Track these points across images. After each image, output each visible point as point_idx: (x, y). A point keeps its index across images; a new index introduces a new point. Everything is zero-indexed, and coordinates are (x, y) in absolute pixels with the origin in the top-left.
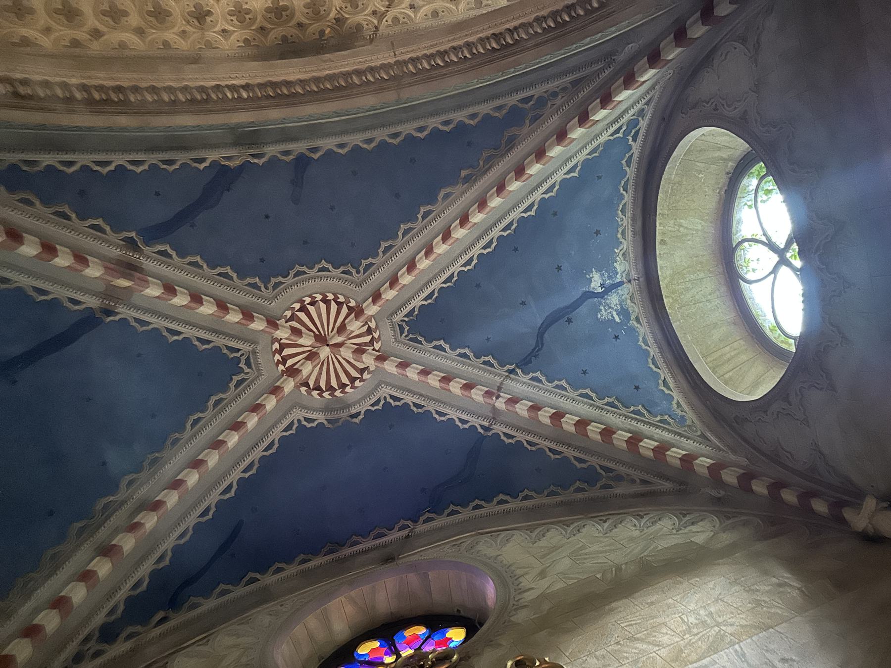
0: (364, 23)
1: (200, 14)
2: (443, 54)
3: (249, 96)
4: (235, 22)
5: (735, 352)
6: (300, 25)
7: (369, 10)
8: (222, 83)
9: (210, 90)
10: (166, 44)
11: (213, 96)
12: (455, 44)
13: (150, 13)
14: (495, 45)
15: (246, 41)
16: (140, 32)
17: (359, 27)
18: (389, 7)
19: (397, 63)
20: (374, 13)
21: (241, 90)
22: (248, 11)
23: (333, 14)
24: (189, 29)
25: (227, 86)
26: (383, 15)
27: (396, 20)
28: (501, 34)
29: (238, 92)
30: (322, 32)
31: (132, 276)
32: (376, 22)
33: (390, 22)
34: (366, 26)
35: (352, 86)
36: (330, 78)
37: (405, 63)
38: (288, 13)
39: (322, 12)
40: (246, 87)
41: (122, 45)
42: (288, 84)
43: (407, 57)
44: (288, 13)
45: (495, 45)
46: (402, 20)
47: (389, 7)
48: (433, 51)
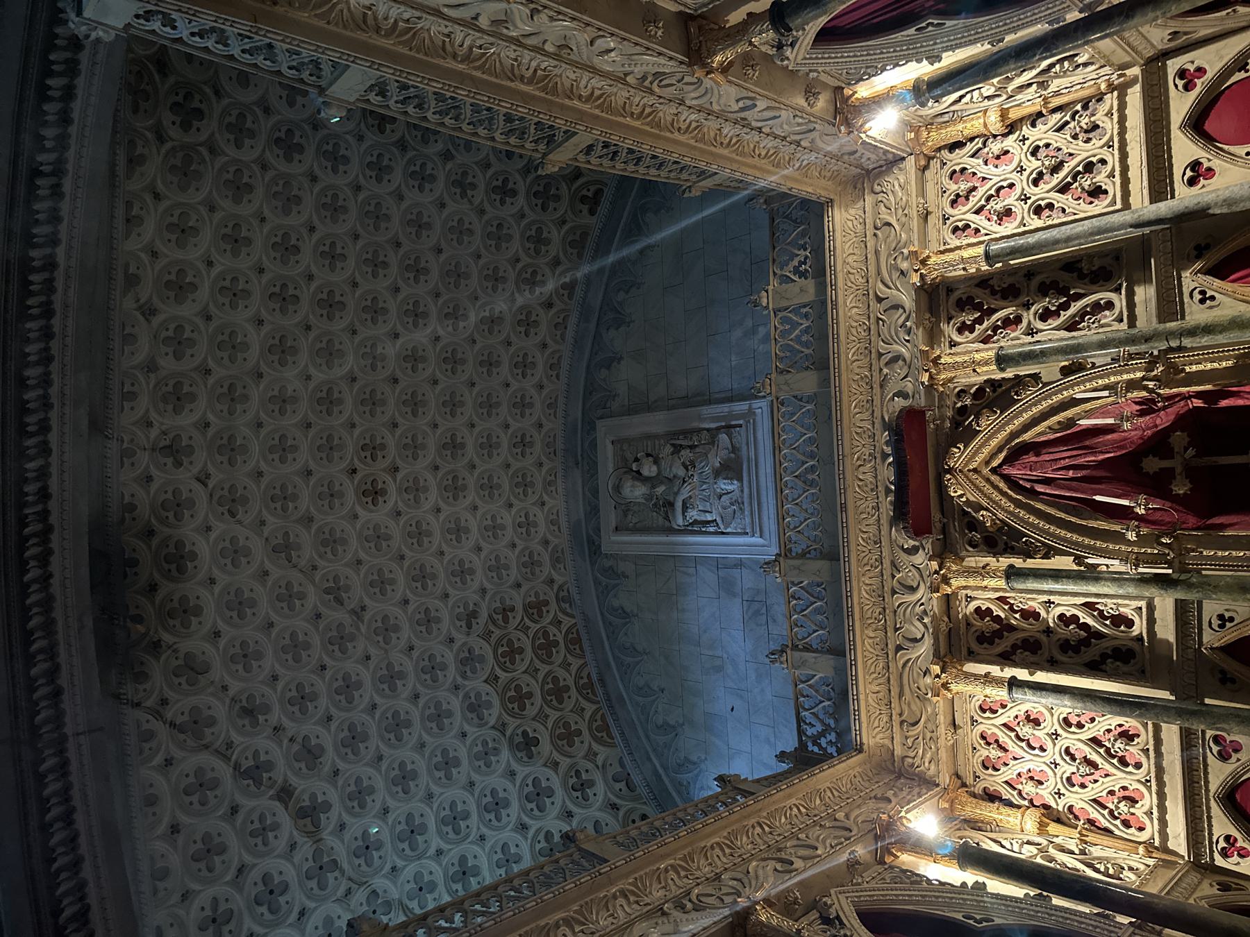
0: (147, 686)
1: (177, 451)
2: (68, 819)
3: (27, 494)
4: (163, 497)
5: (1135, 96)
6: (153, 588)
7: (170, 694)
8: (54, 459)
9: (41, 438)
10: (132, 396)
11: (30, 442)
12: (83, 840)
13: (178, 385)
14: (67, 913)
15: (132, 508)
16: (151, 367)
17: (141, 677)
18: (172, 725)
19: (63, 739)
20: (164, 702)
21: (39, 485)
22: (178, 517)
23: (167, 638)
24: (154, 433)
25: (48, 465)
26: (158, 715)
27: (149, 736)
28: (87, 922)
29: (37, 479)
30: (138, 619)
31: (1230, 205)
32: (149, 703)
33: (145, 726)
34: (141, 687)
35: (30, 660)
36: (49, 627)
37: (61, 752)
38: (175, 573)
39: (171, 622)
40: (44, 495)
41: (130, 339)
42: (44, 559)
43: (71, 754)
44: (175, 573)
45: (67, 913)
46: (146, 746)
47: (172, 725)
48: (77, 801)
